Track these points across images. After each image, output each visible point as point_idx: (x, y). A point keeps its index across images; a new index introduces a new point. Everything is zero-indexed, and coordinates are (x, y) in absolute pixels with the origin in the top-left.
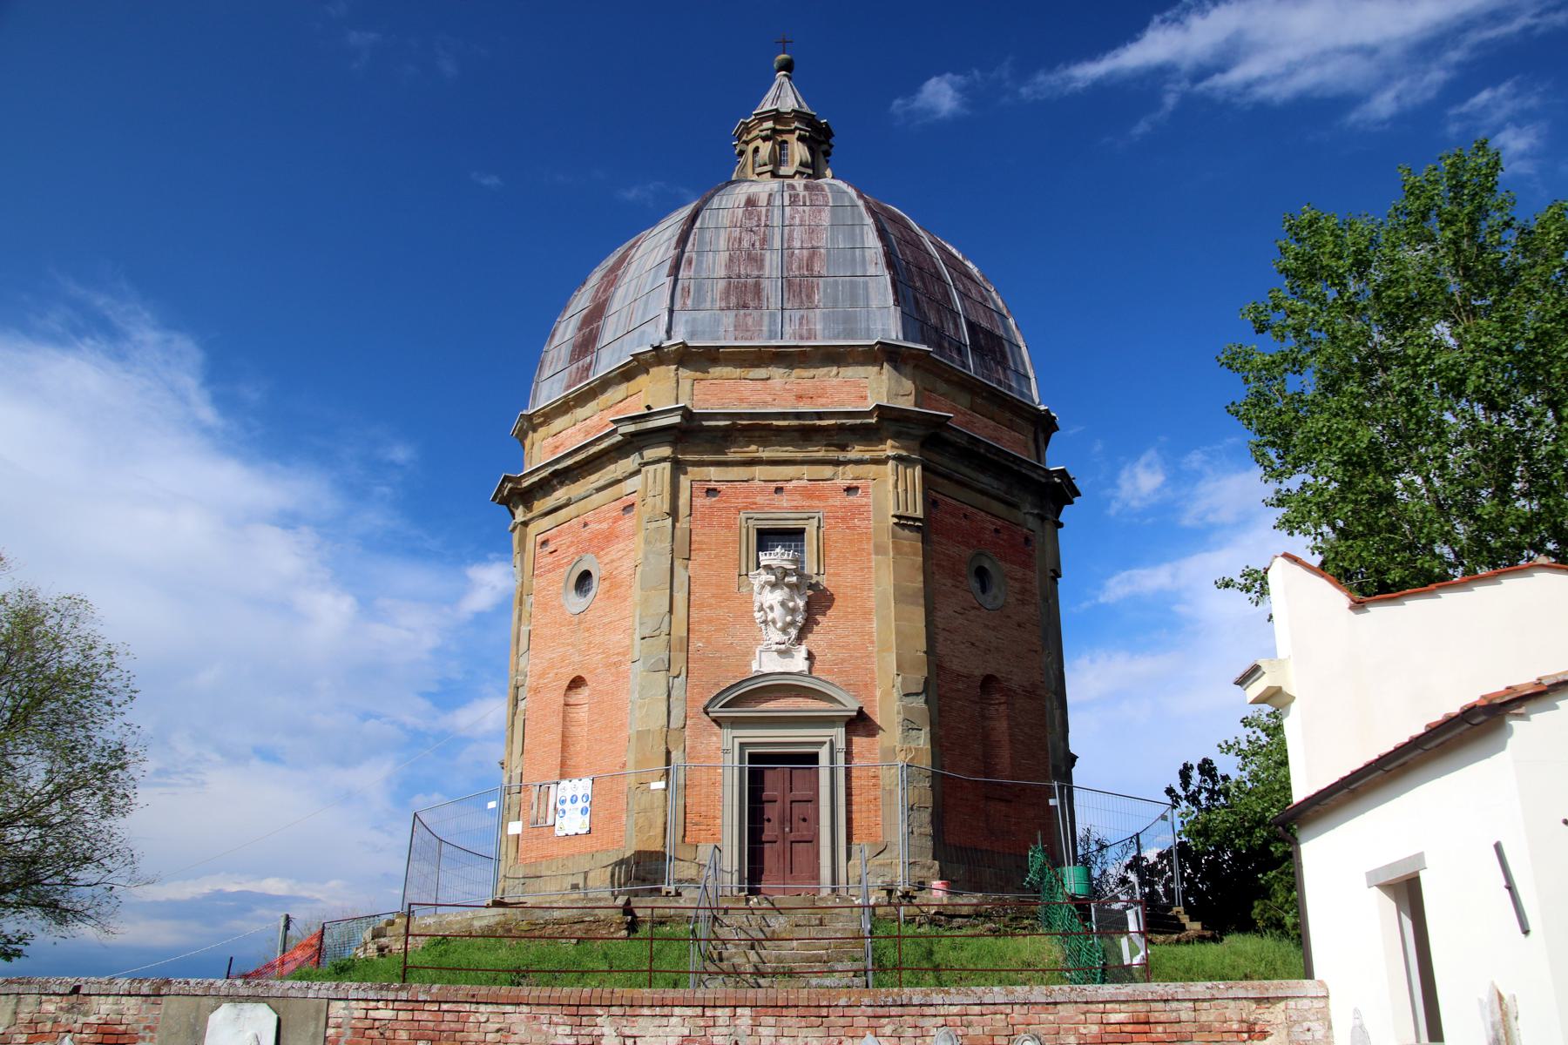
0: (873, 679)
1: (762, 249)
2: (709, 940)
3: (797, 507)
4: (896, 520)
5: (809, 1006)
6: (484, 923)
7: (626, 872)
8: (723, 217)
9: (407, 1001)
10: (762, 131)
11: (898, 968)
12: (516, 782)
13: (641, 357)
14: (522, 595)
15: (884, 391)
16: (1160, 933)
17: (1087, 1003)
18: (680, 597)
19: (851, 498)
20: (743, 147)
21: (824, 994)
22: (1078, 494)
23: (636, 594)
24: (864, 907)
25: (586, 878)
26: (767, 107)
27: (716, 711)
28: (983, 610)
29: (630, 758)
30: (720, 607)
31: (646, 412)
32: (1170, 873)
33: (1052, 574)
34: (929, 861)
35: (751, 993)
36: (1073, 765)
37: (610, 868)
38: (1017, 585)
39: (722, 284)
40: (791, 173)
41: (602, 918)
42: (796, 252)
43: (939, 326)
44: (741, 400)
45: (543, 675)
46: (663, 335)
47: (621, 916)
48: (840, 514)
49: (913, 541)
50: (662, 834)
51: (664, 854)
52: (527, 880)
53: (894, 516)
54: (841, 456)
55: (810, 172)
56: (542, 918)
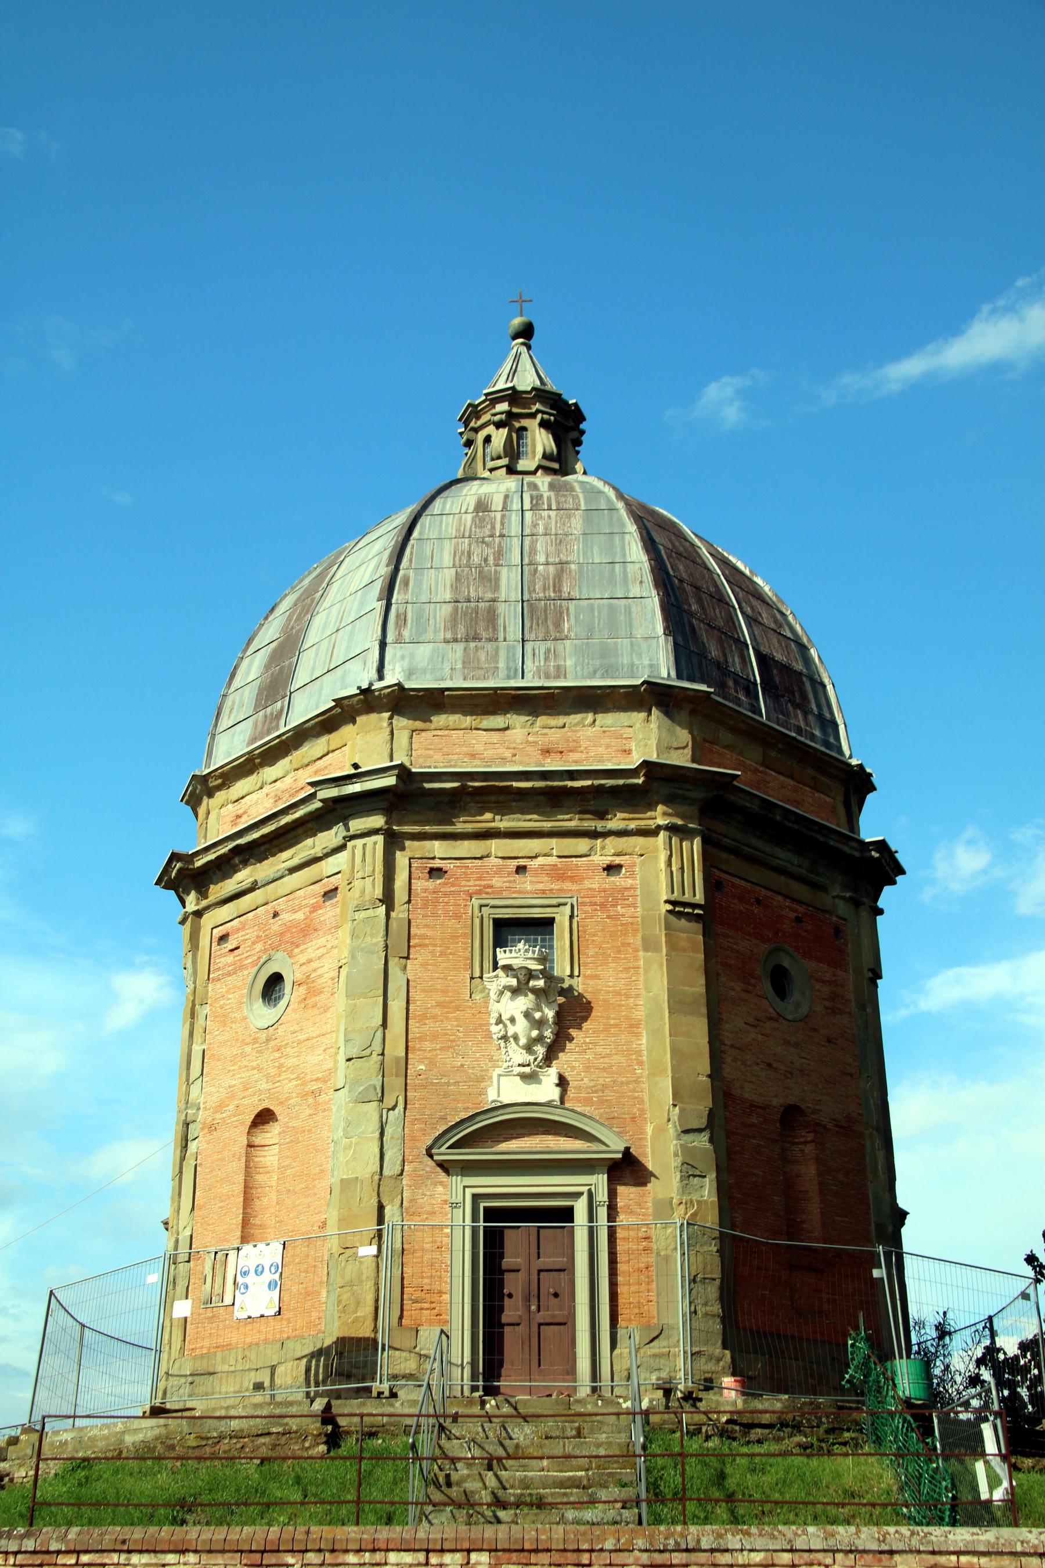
0: (642, 1111)
1: (497, 565)
2: (434, 1459)
3: (544, 891)
4: (669, 907)
5: (565, 1550)
6: (140, 1437)
7: (326, 1366)
8: (447, 524)
9: (35, 1552)
10: (494, 415)
11: (680, 1497)
12: (183, 1249)
13: (346, 702)
14: (194, 1005)
15: (653, 742)
16: (1028, 1455)
17: (933, 1553)
18: (396, 1007)
19: (613, 879)
20: (472, 435)
21: (584, 1534)
22: (903, 872)
23: (340, 1003)
24: (634, 1414)
25: (273, 1374)
26: (501, 385)
27: (443, 1154)
28: (781, 1020)
29: (332, 1216)
30: (447, 1018)
31: (353, 771)
32: (1036, 1372)
33: (870, 975)
34: (718, 1351)
35: (489, 1532)
36: (903, 1224)
37: (305, 1360)
38: (826, 989)
39: (447, 609)
40: (533, 468)
41: (294, 1428)
42: (541, 568)
43: (721, 660)
44: (473, 756)
45: (220, 1107)
46: (374, 675)
47: (319, 1425)
48: (598, 900)
49: (692, 934)
50: (371, 1317)
51: (375, 1341)
52: (196, 1378)
53: (667, 902)
54: (600, 825)
55: (556, 466)
56: (215, 1430)
